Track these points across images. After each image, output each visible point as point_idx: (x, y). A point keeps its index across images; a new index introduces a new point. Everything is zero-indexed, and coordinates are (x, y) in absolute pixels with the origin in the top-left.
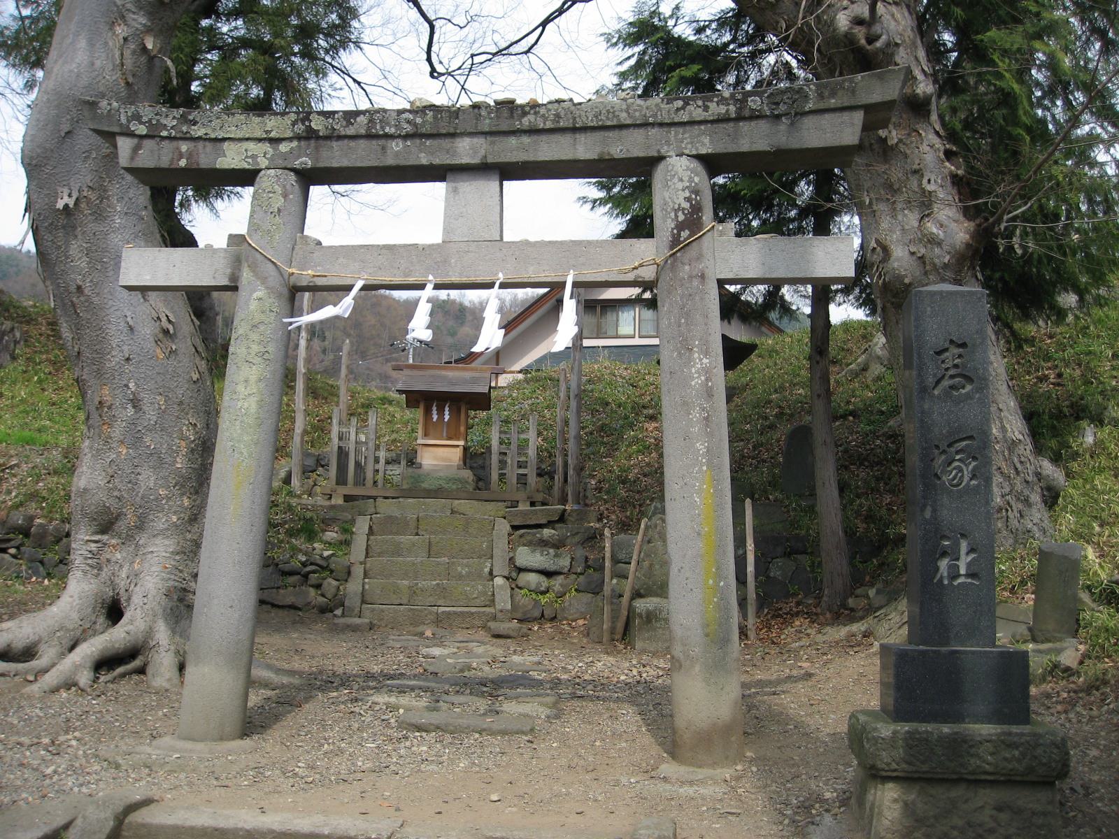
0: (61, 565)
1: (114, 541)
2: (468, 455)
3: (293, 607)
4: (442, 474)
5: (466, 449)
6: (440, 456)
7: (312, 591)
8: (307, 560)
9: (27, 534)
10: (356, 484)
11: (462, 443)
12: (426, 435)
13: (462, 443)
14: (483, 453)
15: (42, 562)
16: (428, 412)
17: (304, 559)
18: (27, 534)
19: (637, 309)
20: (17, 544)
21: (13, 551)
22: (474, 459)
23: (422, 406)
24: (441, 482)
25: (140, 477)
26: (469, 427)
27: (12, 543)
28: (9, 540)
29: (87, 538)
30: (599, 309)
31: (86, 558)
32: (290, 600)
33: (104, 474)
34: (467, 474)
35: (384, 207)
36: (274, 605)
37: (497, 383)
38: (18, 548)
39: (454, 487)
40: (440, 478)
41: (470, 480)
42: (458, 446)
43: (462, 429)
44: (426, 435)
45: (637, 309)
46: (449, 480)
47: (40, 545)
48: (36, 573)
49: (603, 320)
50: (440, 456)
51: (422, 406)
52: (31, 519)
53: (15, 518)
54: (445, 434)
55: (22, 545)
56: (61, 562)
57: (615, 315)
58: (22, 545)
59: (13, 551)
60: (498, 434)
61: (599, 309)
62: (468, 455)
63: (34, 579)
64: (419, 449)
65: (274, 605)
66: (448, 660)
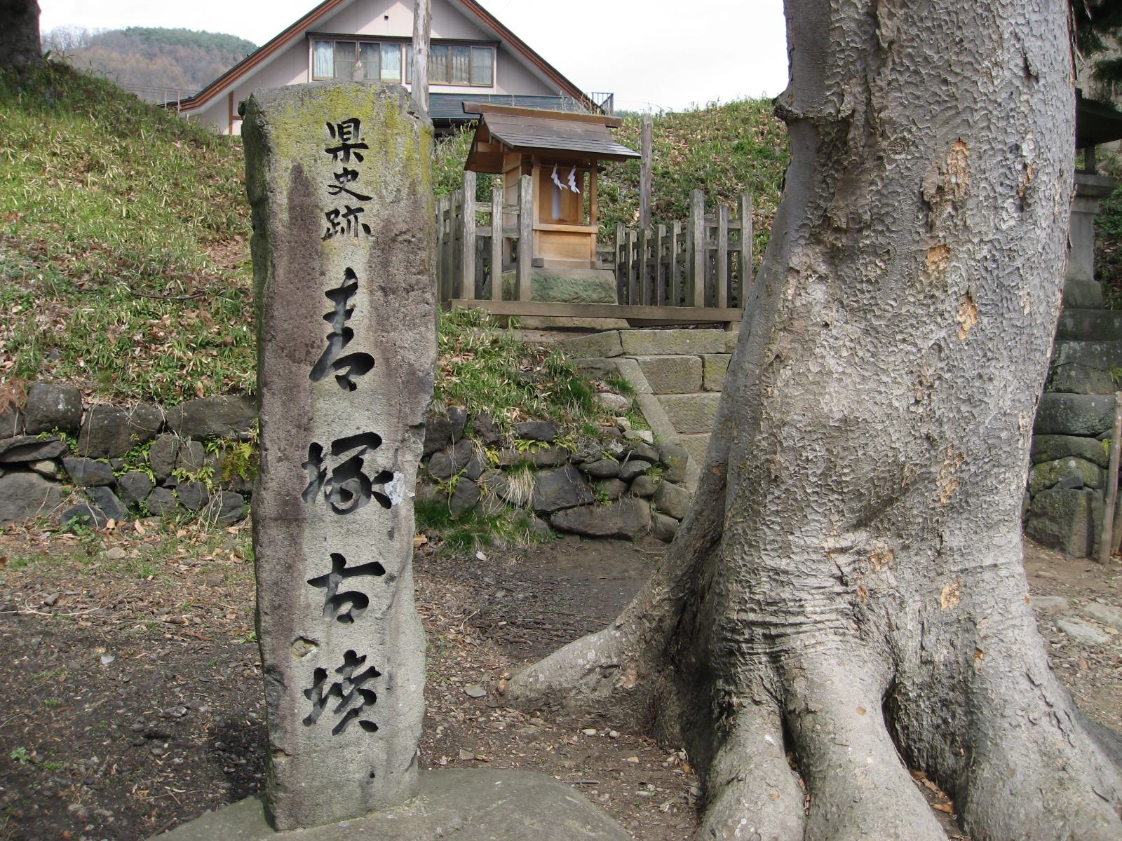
0: (160, 489)
1: (880, 544)
3: (621, 537)
7: (645, 507)
8: (626, 451)
9: (74, 431)
15: (113, 486)
16: (545, 180)
17: (619, 449)
18: (74, 431)
19: (404, 50)
20: (57, 453)
21: (48, 467)
23: (536, 172)
24: (577, 289)
25: (989, 386)
27: (45, 451)
28: (38, 446)
29: (831, 543)
31: (831, 597)
32: (614, 525)
33: (908, 380)
36: (584, 536)
37: (231, 131)
38: (58, 460)
39: (595, 296)
42: (589, 234)
47: (106, 452)
48: (109, 510)
51: (536, 172)
52: (75, 397)
53: (50, 398)
55: (68, 451)
56: (160, 483)
58: (68, 451)
59: (48, 467)
63: (111, 523)
65: (584, 536)
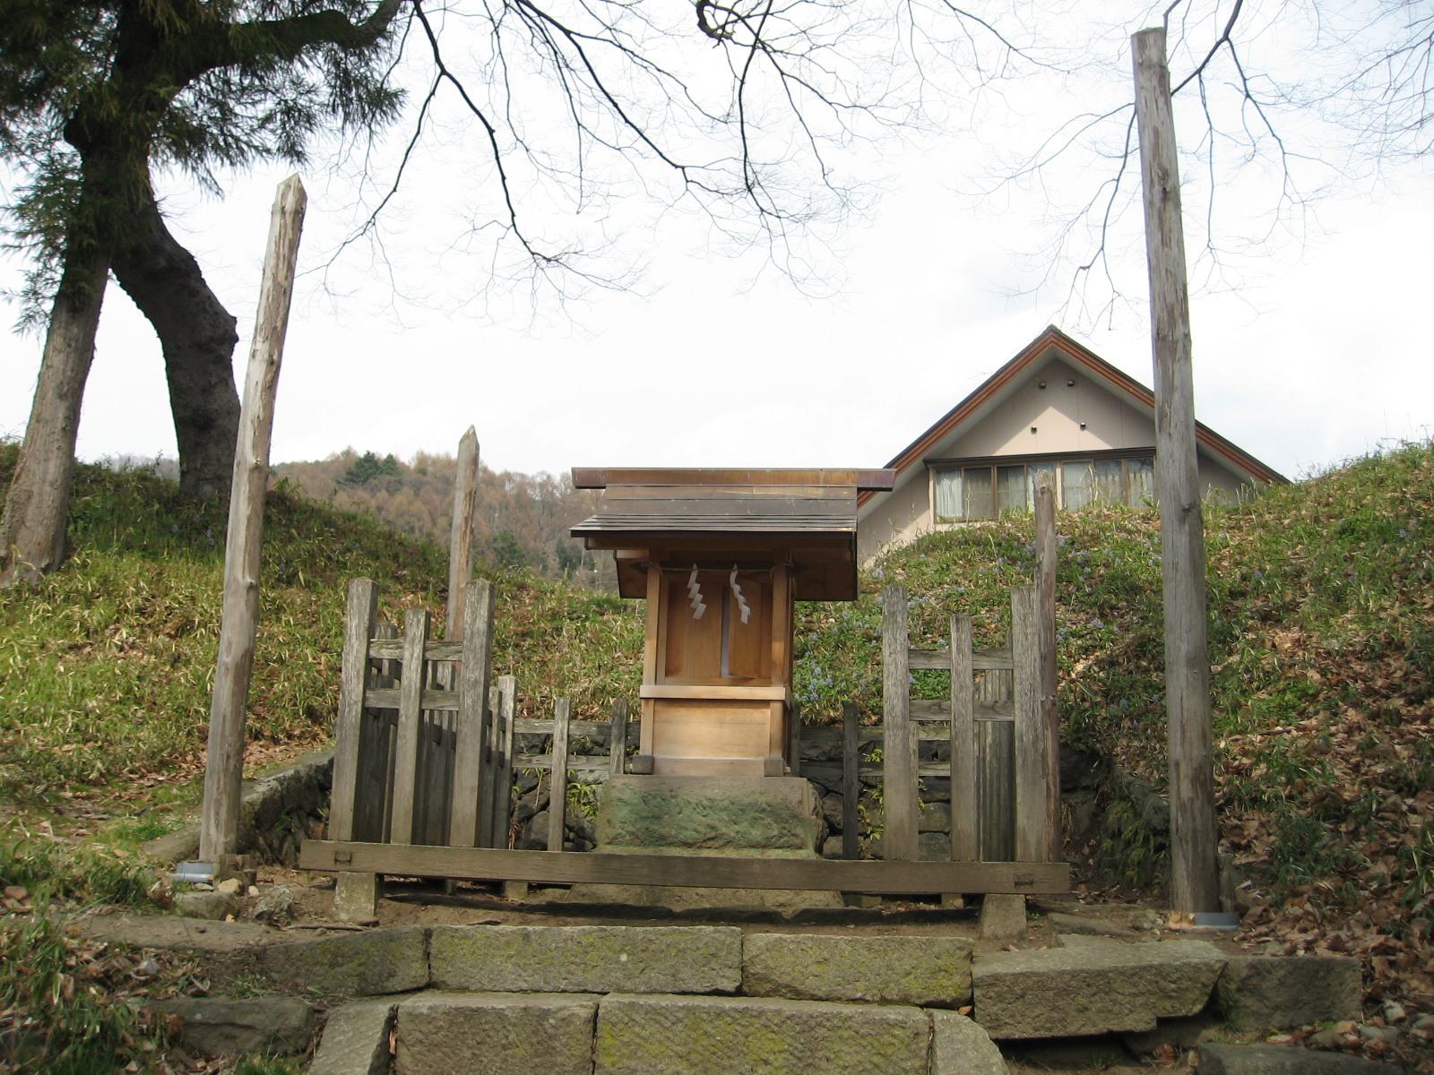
2: (796, 728)
4: (715, 793)
5: (789, 710)
6: (717, 740)
10: (421, 834)
11: (776, 692)
12: (670, 669)
13: (776, 692)
14: (833, 721)
19: (1058, 471)
22: (823, 747)
24: (713, 819)
26: (794, 654)
30: (994, 472)
34: (799, 792)
35: (624, 283)
40: (712, 805)
41: (807, 811)
43: (778, 648)
44: (670, 669)
45: (1058, 471)
46: (739, 811)
49: (1002, 491)
50: (717, 740)
54: (725, 670)
57: (1021, 480)
60: (902, 659)
61: (994, 472)
62: (796, 728)
64: (646, 713)
66: (744, 619)
